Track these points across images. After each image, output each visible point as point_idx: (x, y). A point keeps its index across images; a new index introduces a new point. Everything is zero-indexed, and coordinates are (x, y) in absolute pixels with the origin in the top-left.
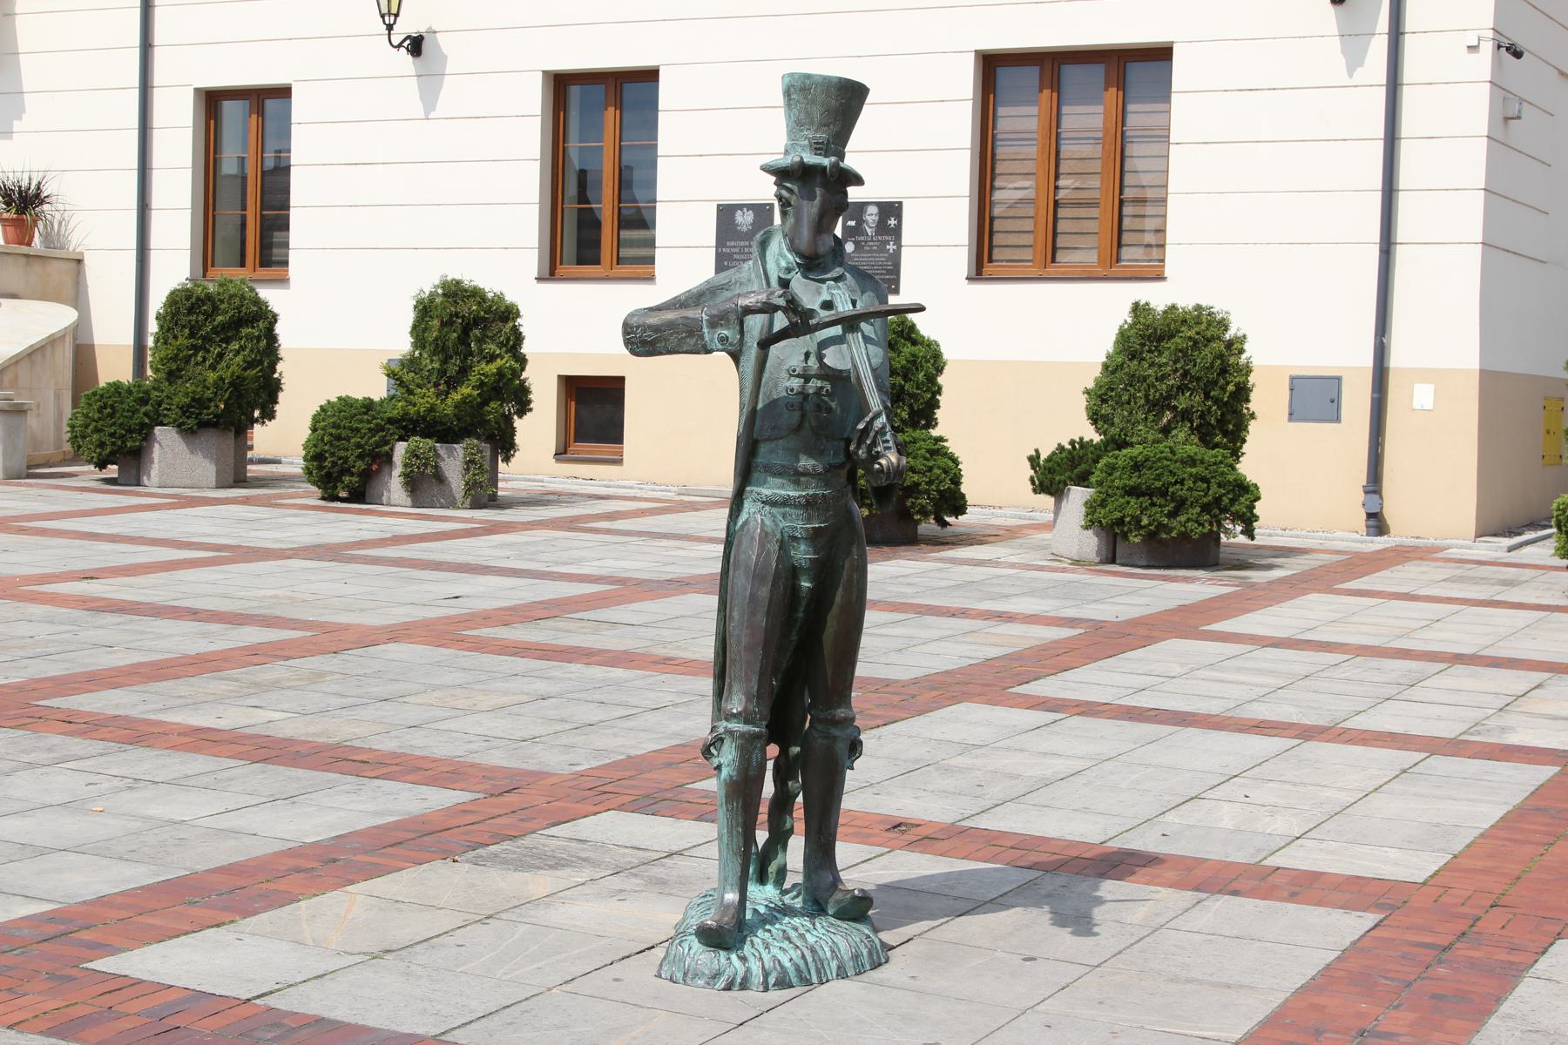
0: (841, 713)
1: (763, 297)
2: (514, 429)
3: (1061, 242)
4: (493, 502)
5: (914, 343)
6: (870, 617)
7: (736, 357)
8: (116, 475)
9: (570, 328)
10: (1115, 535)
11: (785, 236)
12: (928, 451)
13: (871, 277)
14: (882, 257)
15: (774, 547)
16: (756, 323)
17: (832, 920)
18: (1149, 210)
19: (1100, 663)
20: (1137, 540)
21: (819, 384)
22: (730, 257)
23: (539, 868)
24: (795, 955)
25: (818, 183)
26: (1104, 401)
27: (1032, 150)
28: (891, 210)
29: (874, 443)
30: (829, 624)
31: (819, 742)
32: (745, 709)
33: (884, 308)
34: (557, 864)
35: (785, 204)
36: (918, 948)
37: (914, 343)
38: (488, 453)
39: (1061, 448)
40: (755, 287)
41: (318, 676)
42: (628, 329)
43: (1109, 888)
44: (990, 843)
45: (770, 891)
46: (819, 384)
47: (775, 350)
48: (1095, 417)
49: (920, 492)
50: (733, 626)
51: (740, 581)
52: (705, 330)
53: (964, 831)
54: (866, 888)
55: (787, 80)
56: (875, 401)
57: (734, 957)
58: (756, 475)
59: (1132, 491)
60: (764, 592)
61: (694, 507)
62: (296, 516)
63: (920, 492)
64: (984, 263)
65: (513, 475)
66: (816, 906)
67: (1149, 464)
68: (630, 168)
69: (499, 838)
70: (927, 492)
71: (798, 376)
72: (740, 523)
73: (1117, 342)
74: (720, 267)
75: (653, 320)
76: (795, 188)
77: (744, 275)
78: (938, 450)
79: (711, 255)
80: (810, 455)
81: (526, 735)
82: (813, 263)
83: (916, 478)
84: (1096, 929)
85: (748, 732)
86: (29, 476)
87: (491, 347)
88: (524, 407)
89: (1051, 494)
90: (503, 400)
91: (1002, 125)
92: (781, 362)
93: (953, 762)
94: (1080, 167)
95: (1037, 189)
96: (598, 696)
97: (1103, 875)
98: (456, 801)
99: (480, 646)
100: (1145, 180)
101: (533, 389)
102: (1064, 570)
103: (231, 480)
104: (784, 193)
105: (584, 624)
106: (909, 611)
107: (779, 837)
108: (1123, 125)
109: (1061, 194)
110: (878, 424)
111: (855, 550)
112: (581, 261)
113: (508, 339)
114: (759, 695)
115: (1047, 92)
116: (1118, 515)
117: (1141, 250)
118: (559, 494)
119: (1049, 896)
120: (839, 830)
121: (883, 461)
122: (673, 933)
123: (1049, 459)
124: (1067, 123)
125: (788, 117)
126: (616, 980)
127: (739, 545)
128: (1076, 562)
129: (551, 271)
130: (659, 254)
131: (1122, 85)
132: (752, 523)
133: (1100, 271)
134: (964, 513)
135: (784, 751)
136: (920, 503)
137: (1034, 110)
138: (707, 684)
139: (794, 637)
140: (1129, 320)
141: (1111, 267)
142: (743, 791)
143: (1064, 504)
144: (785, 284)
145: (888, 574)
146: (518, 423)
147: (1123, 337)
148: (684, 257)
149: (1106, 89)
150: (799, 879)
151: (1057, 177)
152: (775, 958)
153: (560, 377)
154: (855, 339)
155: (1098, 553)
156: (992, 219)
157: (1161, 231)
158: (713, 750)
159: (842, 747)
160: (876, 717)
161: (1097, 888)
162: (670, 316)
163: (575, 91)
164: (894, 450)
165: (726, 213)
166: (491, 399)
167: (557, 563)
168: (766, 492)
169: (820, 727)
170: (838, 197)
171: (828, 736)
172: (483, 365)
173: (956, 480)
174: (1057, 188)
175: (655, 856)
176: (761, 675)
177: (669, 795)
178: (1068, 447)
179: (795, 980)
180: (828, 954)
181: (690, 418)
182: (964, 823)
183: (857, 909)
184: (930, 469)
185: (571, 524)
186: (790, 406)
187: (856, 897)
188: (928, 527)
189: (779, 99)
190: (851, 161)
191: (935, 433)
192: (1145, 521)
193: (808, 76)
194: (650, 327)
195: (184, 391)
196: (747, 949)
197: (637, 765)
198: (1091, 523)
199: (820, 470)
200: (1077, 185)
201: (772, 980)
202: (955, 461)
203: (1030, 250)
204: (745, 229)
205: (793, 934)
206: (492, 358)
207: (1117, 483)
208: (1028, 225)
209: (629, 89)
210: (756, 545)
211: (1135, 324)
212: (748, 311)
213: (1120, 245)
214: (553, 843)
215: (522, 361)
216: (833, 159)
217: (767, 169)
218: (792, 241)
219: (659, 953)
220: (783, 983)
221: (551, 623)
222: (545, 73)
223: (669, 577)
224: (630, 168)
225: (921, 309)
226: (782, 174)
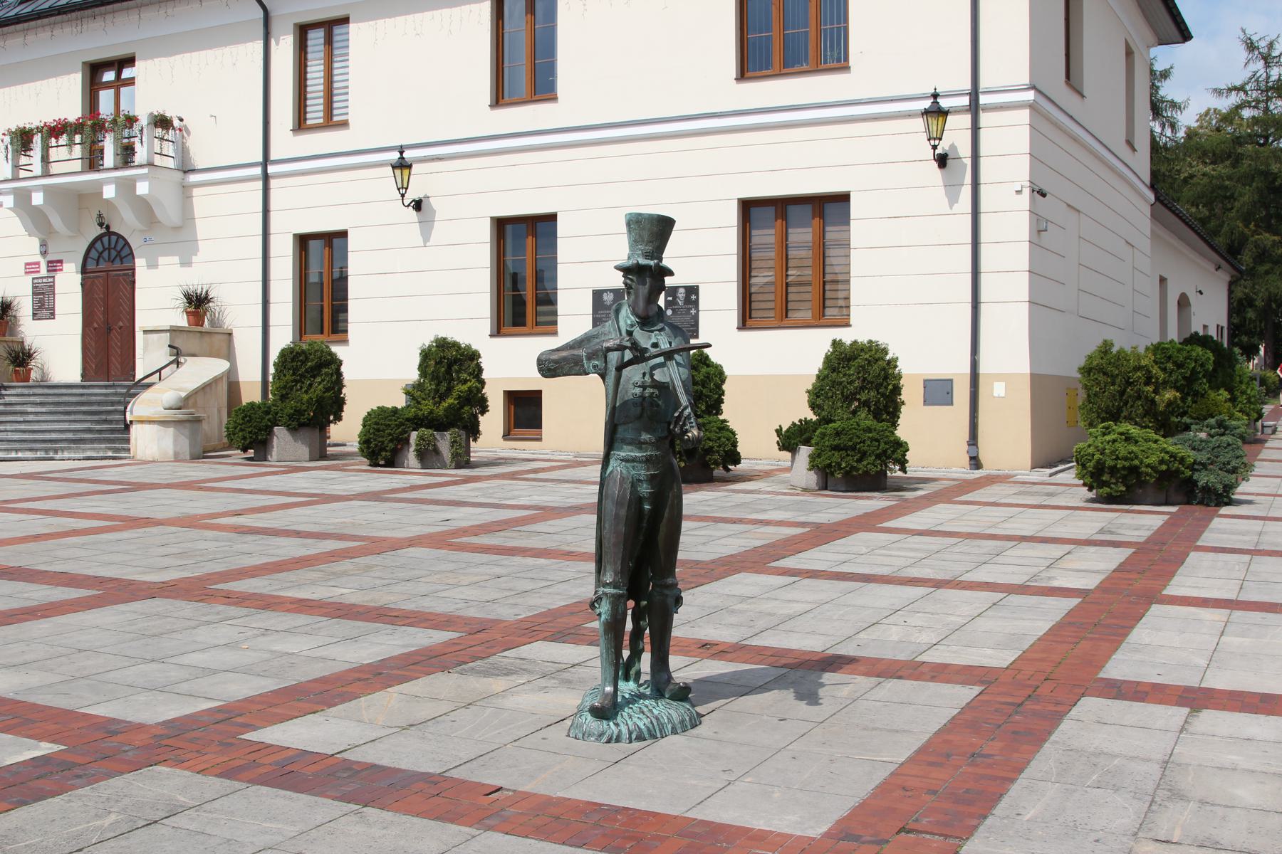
0: (670, 581)
1: (617, 342)
3: (790, 306)
4: (468, 464)
5: (708, 366)
7: (603, 376)
9: (508, 363)
14: (688, 318)
15: (628, 486)
16: (614, 357)
18: (840, 287)
24: (647, 721)
25: (647, 275)
27: (772, 254)
28: (692, 291)
29: (684, 424)
34: (509, 673)
36: (719, 717)
37: (708, 366)
39: (794, 424)
41: (369, 568)
42: (540, 362)
43: (828, 677)
45: (631, 685)
47: (625, 372)
48: (813, 406)
51: (609, 507)
56: (684, 400)
58: (616, 445)
59: (836, 448)
60: (623, 512)
61: (583, 464)
64: (747, 319)
66: (658, 693)
74: (595, 325)
75: (554, 357)
77: (606, 329)
80: (648, 432)
87: (464, 376)
88: (484, 410)
91: (755, 240)
93: (736, 607)
96: (530, 575)
97: (824, 670)
100: (837, 269)
106: (708, 523)
107: (636, 654)
109: (790, 279)
112: (515, 325)
114: (622, 572)
115: (779, 221)
123: (788, 431)
124: (792, 238)
125: (629, 238)
128: (805, 490)
129: (498, 331)
130: (560, 319)
135: (637, 604)
136: (714, 458)
137: (773, 231)
138: (592, 566)
141: (820, 319)
142: (614, 627)
144: (630, 333)
145: (695, 500)
146: (481, 418)
147: (828, 359)
150: (648, 678)
154: (672, 365)
157: (848, 298)
159: (670, 601)
162: (564, 354)
163: (509, 228)
168: (623, 454)
173: (735, 444)
183: (682, 694)
185: (512, 476)
186: (635, 404)
188: (719, 472)
189: (624, 229)
190: (666, 262)
191: (721, 417)
193: (640, 214)
196: (619, 719)
197: (552, 614)
202: (734, 434)
205: (645, 710)
206: (465, 382)
208: (772, 297)
212: (609, 350)
213: (824, 307)
215: (483, 383)
217: (617, 268)
219: (568, 722)
220: (640, 738)
221: (502, 534)
225: (709, 346)
226: (626, 271)
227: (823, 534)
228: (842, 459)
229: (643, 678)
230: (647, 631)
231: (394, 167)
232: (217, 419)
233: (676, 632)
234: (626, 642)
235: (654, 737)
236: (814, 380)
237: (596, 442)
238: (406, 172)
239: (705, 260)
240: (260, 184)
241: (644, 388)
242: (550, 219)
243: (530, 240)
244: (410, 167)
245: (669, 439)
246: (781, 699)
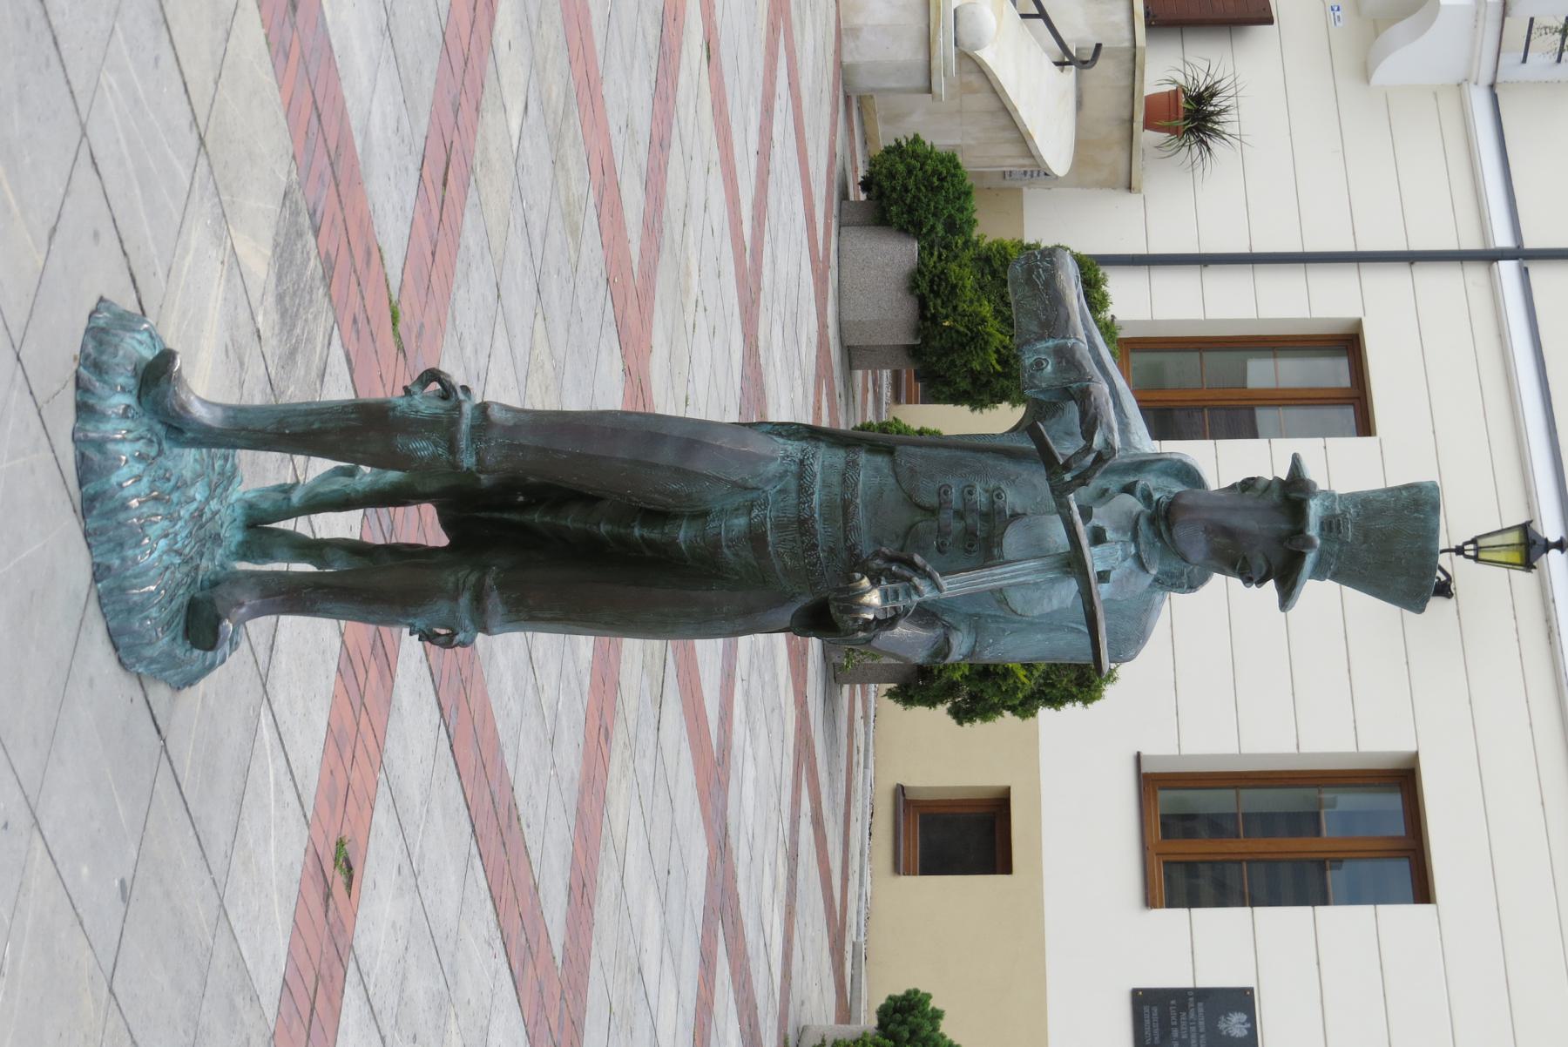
0: (494, 602)
8: (852, 198)
41: (575, 231)
52: (1051, 343)
62: (805, 396)
86: (847, 99)
101: (989, 724)
103: (852, 342)
146: (942, 709)
167: (747, 693)
187: (218, 620)
190: (1317, 593)
195: (966, 277)
204: (1222, 1026)
209: (1400, 870)
220: (85, 469)
222: (1415, 757)
231: (1525, 528)
232: (941, 130)
238: (1515, 557)
240: (1472, 243)
244: (1528, 565)
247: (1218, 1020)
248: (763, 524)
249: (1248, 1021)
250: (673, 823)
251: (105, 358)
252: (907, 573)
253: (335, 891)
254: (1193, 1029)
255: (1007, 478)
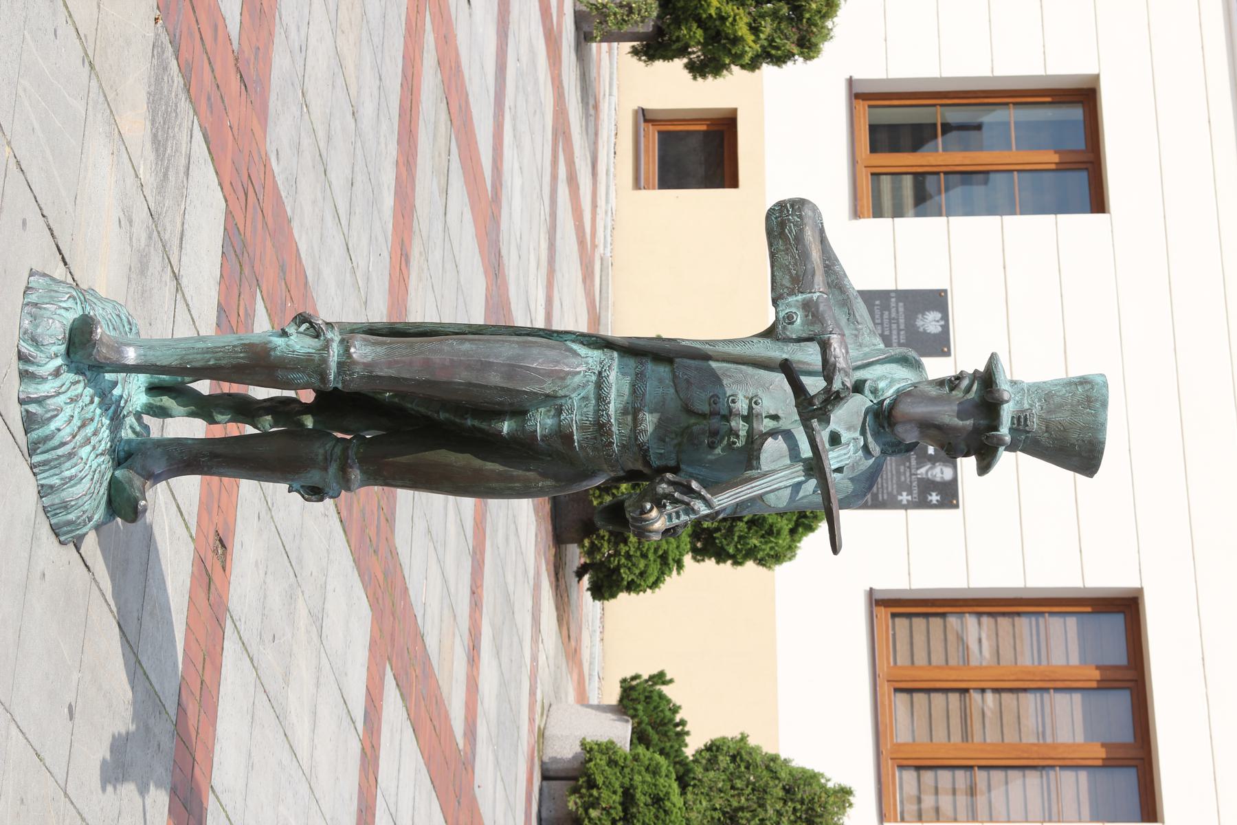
0: (356, 474)
1: (841, 363)
2: (671, 58)
3: (920, 698)
4: (584, 37)
5: (793, 532)
6: (468, 503)
7: (770, 333)
9: (794, 122)
10: (575, 779)
11: (915, 386)
12: (666, 552)
13: (871, 487)
14: (892, 487)
15: (548, 388)
16: (810, 355)
17: (108, 476)
18: (962, 800)
19: (424, 771)
20: (571, 806)
21: (743, 433)
22: (886, 307)
23: (153, 122)
24: (65, 434)
25: (977, 422)
26: (733, 758)
27: (1026, 660)
28: (948, 496)
29: (675, 501)
30: (460, 456)
31: (319, 450)
32: (355, 363)
33: (835, 505)
34: (159, 144)
35: (952, 383)
36: (76, 581)
37: (793, 532)
38: (641, 29)
39: (675, 710)
40: (853, 353)
42: (798, 205)
43: (159, 799)
44: (207, 656)
45: (140, 399)
46: (743, 433)
47: (780, 379)
48: (713, 749)
49: (616, 544)
50: (452, 344)
51: (505, 351)
52: (800, 297)
53: (219, 623)
54: (147, 514)
55: (1099, 380)
56: (724, 500)
57: (59, 362)
58: (631, 362)
59: (628, 796)
60: (495, 379)
61: (587, 276)
63: (616, 544)
64: (891, 607)
65: (617, 61)
66: (123, 456)
67: (662, 814)
68: (986, 182)
69: (186, 72)
70: (617, 553)
71: (750, 408)
72: (575, 346)
73: (804, 771)
74: (870, 297)
75: (809, 235)
76: (972, 395)
77: (867, 339)
78: (668, 562)
79: (884, 283)
80: (659, 426)
81: (310, 96)
82: (883, 419)
83: (633, 539)
84: (110, 788)
85: (328, 367)
87: (767, 27)
88: (698, 69)
89: (621, 700)
90: (704, 45)
91: (1055, 624)
92: (766, 388)
93: (301, 603)
94: (1009, 718)
95: (981, 667)
96: (359, 178)
97: (174, 792)
98: (228, 16)
99: (413, 34)
100: (997, 795)
101: (720, 80)
102: (532, 720)
104: (965, 383)
105: (444, 156)
106: (475, 550)
107: (204, 408)
108: (1062, 767)
109: (976, 696)
110: (699, 506)
111: (549, 483)
112: (873, 129)
113: (777, 48)
114: (372, 378)
115: (1096, 675)
116: (600, 780)
117: (914, 792)
118: (596, 107)
119: (147, 729)
120: (215, 479)
121: (654, 513)
122: (84, 286)
123: (662, 696)
124: (1061, 699)
125: (1055, 383)
126: (24, 223)
127: (548, 346)
128: (542, 734)
129: (859, 95)
130: (885, 222)
131: (1110, 763)
132: (575, 361)
133: (887, 748)
134: (594, 598)
135: (307, 409)
136: (605, 546)
137: (1075, 660)
138: (379, 314)
139: (443, 416)
140: (830, 785)
141: (893, 760)
142: (258, 363)
143: (610, 716)
144: (858, 388)
145: (520, 522)
146: (679, 63)
147: (810, 778)
148: (878, 253)
149: (1103, 745)
150: (155, 434)
151: (996, 690)
152: (59, 410)
153: (735, 111)
154: (797, 473)
155: (554, 760)
156: (943, 615)
157: (937, 814)
158: (304, 326)
159: (314, 477)
160: (350, 510)
161: (159, 785)
162: (815, 255)
163: (1076, 113)
164: (668, 525)
165: (937, 300)
166: (705, 30)
167: (514, 118)
168: (613, 376)
169: (338, 450)
170: (963, 446)
171: (327, 460)
172: (746, 19)
173: (631, 587)
174: (983, 690)
175: (174, 261)
176: (397, 380)
177: (247, 271)
178: (677, 719)
179: (33, 435)
180: (67, 474)
181: (689, 274)
182: (229, 623)
183: (122, 504)
184: (644, 556)
185: (561, 132)
186: (714, 399)
187: (136, 502)
188: (576, 555)
189: (1076, 372)
190: (1006, 460)
191: (688, 559)
192: (594, 813)
193: (1104, 405)
194: (801, 231)
196: (68, 377)
197: (280, 228)
198: (589, 750)
199: (642, 438)
200: (988, 713)
201: (33, 408)
202: (654, 585)
203: (908, 663)
204: (919, 323)
205: (89, 430)
206: (755, 30)
207: (637, 778)
208: (938, 659)
209: (1080, 179)
210: (550, 367)
211: (827, 791)
212: (825, 346)
213: (918, 768)
214: (184, 138)
215: (753, 66)
216: (1008, 439)
217: (993, 359)
218: (908, 394)
219: (59, 272)
220: (30, 422)
221: (444, 116)
222: (1097, 78)
223: (504, 252)
224: (986, 182)
225: (835, 549)
226: (987, 379)
227: (451, 774)
228: (607, 810)
229: (152, 422)
230: (250, 430)
233: (248, 488)
234: (227, 387)
235: (32, 451)
236: (768, 749)
237: (629, 324)
239: (1006, 528)
241: (748, 418)
242: (1097, 201)
243: (1051, 158)
245: (644, 472)
246: (112, 705)
247: (915, 319)
248: (571, 427)
249: (942, 319)
250: (458, 282)
251: (39, 330)
252: (686, 499)
253: (214, 577)
254: (894, 326)
255: (763, 386)
